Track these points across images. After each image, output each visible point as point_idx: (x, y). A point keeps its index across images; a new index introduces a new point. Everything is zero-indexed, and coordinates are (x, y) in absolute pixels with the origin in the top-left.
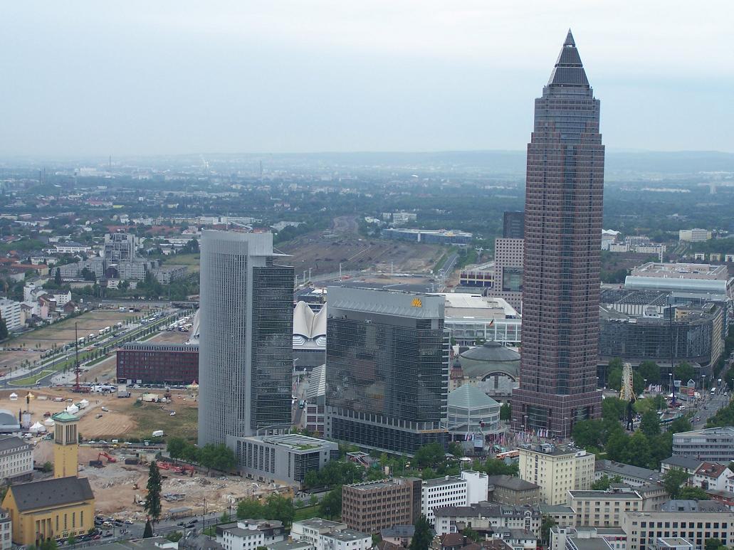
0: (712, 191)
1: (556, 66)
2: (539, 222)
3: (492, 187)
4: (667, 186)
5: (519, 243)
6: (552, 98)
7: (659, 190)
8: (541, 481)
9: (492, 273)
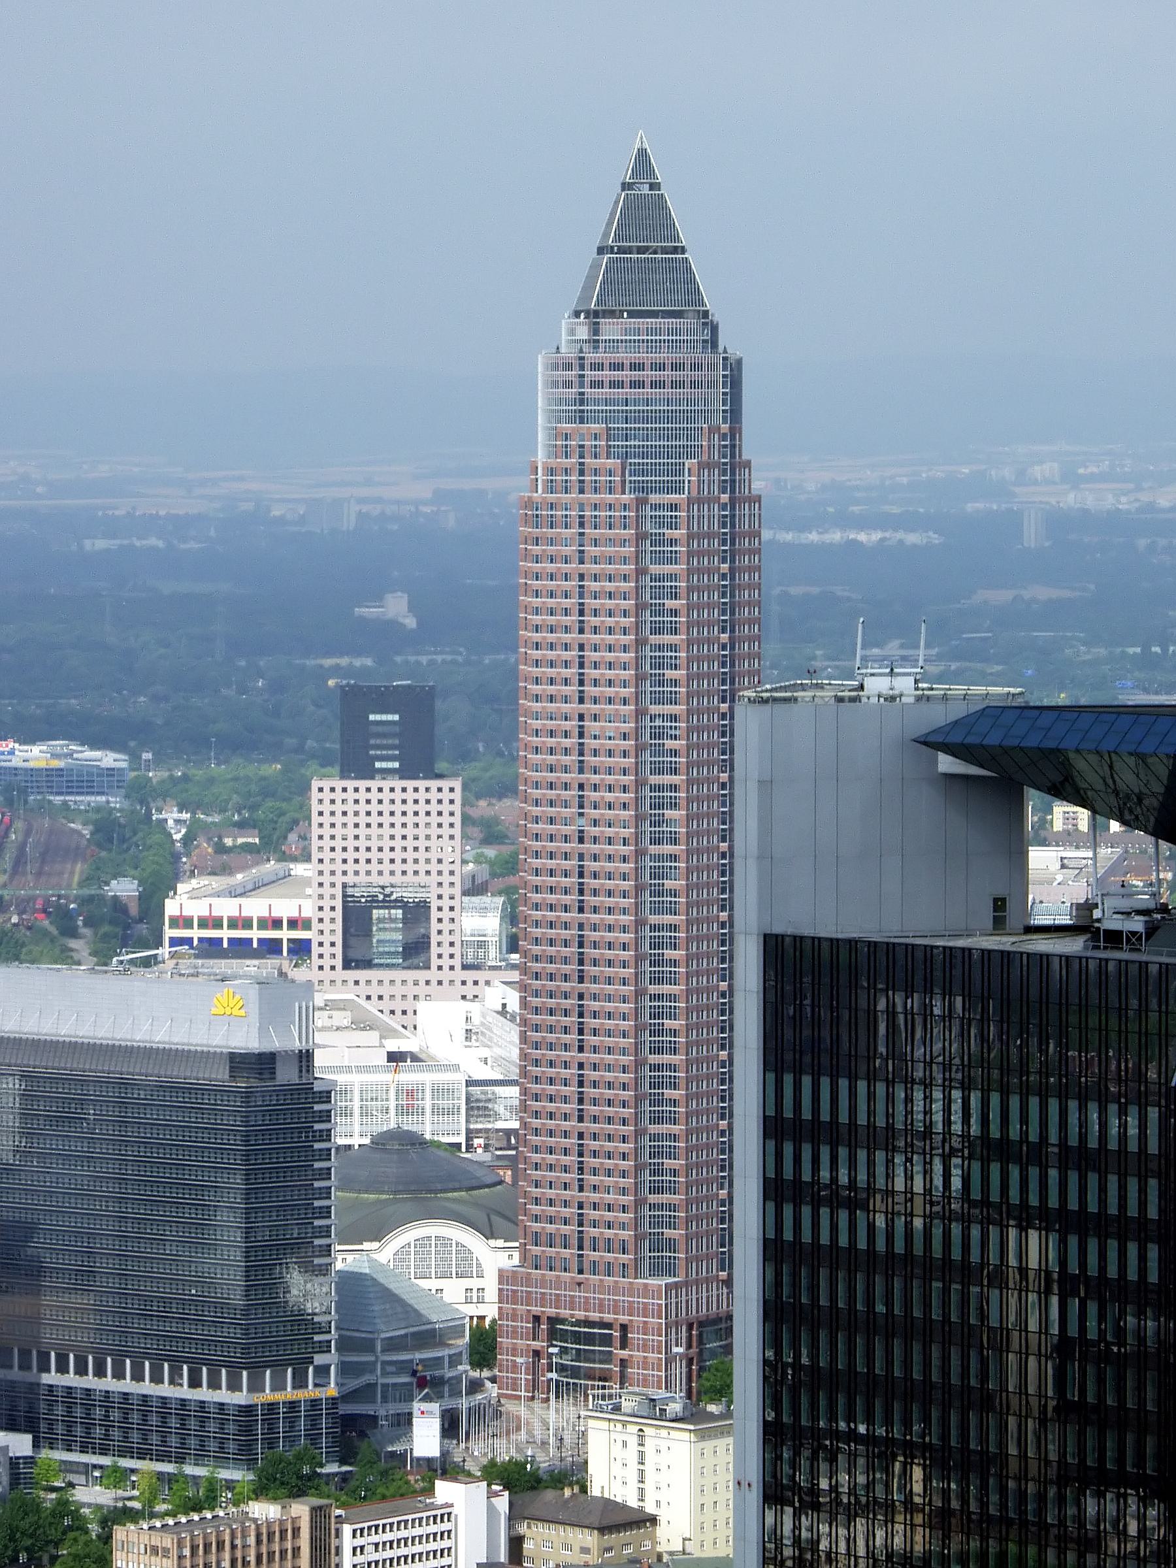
0: (1032, 535)
1: (601, 251)
2: (567, 742)
3: (113, 544)
4: (845, 521)
5: (327, 796)
6: (590, 356)
7: (813, 537)
8: (658, 1503)
9: (308, 910)
